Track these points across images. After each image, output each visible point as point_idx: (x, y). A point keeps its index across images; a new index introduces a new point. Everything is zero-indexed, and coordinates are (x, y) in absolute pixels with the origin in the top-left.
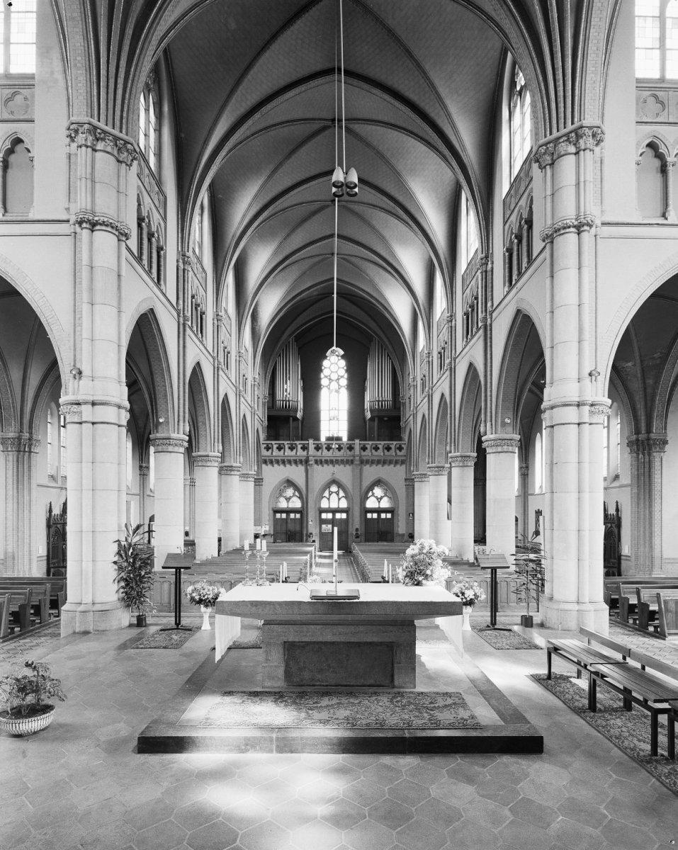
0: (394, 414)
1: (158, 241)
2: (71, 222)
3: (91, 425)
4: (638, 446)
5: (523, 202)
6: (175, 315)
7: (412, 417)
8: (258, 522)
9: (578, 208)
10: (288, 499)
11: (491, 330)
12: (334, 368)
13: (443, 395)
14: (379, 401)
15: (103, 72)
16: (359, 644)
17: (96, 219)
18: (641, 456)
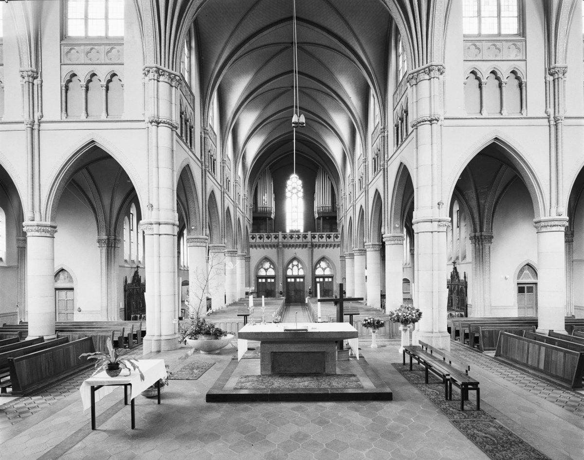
0: (333, 215)
1: (190, 124)
2: (146, 122)
3: (158, 236)
4: (475, 239)
5: (403, 100)
6: (200, 165)
7: (343, 218)
8: (248, 284)
9: (431, 111)
10: (266, 270)
11: (387, 171)
12: (294, 185)
13: (361, 206)
14: (323, 207)
15: (163, 38)
16: (308, 353)
17: (160, 120)
18: (477, 245)
